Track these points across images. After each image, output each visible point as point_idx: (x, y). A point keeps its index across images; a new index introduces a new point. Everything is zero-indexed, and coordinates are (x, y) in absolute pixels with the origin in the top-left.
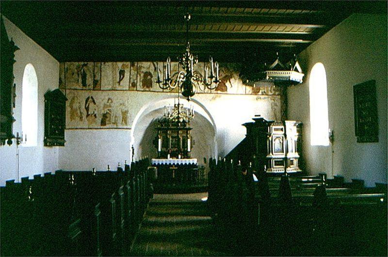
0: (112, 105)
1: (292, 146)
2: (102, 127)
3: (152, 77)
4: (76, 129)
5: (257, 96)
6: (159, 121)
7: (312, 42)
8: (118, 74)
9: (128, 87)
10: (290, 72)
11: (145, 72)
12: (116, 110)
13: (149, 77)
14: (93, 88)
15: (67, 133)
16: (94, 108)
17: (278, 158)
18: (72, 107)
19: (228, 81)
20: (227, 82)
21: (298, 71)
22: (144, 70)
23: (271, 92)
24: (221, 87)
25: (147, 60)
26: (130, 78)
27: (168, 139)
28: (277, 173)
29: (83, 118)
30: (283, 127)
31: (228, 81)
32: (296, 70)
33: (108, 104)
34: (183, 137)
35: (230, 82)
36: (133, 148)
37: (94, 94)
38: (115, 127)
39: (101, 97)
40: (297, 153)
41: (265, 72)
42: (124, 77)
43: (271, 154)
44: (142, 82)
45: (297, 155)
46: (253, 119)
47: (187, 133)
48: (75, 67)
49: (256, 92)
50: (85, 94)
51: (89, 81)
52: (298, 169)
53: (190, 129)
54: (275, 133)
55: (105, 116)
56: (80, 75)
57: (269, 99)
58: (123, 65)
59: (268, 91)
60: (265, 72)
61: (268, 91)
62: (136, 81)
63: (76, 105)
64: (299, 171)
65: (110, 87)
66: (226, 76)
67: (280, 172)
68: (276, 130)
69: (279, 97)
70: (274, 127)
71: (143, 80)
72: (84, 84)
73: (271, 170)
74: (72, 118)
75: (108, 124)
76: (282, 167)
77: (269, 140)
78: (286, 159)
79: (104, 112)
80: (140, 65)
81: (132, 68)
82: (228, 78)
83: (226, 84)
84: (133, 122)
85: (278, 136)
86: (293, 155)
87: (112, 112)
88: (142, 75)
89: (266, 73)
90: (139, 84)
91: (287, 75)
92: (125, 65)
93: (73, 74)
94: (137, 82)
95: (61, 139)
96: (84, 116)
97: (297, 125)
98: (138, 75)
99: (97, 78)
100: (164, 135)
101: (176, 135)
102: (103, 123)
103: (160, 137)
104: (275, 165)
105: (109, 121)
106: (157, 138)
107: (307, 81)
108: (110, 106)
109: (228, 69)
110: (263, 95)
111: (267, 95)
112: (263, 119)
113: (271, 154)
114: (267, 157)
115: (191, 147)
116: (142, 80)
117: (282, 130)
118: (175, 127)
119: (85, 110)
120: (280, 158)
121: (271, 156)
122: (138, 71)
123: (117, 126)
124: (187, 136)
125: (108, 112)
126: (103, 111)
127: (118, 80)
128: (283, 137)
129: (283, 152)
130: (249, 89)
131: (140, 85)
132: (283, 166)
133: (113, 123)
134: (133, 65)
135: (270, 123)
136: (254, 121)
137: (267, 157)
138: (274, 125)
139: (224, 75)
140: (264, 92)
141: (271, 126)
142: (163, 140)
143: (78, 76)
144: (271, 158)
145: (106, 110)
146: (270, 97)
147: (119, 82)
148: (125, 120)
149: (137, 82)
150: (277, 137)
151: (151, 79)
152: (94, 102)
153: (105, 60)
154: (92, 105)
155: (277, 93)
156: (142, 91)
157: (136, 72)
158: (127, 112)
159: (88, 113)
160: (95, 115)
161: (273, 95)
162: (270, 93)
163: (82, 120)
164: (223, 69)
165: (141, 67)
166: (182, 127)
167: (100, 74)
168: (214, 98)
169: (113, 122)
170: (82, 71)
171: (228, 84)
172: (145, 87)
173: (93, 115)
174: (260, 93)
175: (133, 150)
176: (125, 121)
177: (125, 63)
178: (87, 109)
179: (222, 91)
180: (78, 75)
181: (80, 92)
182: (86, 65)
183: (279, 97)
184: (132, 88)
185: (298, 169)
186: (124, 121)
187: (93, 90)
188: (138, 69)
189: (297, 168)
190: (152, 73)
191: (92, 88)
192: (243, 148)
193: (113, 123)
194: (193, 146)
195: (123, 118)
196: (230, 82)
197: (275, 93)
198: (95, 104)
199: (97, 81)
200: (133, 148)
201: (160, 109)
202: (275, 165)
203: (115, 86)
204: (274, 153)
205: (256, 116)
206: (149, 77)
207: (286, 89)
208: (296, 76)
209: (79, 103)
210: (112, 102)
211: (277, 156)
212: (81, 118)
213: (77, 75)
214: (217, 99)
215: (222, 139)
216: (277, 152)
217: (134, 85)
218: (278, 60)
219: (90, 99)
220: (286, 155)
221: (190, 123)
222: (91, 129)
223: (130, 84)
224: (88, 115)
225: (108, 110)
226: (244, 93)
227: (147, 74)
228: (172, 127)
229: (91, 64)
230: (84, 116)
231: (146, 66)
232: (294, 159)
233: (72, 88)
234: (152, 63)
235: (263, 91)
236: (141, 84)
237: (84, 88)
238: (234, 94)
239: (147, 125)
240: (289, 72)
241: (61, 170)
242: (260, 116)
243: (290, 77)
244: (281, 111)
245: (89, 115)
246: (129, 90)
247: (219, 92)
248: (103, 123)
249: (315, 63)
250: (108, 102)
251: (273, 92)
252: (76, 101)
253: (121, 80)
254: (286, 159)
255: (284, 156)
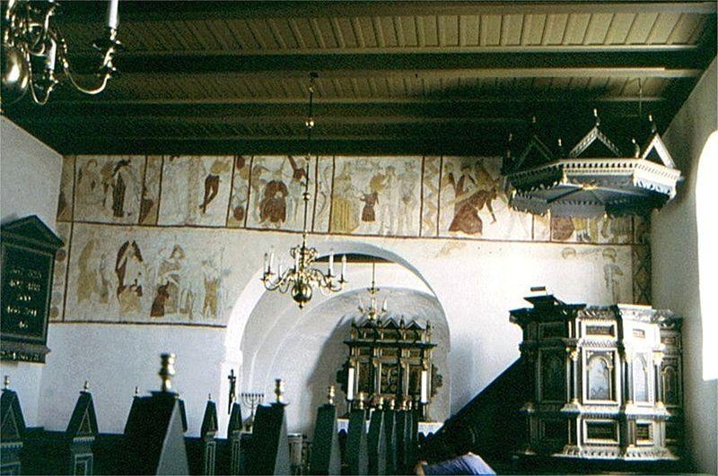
0: (183, 262)
1: (644, 379)
2: (153, 319)
3: (286, 194)
4: (90, 322)
5: (565, 246)
6: (354, 325)
7: (695, 71)
8: (202, 185)
9: (225, 220)
10: (633, 161)
11: (269, 181)
12: (191, 279)
13: (279, 194)
14: (141, 219)
15: (55, 333)
16: (139, 270)
17: (598, 416)
18: (83, 266)
19: (485, 205)
20: (481, 208)
21: (660, 162)
22: (267, 176)
23: (605, 236)
24: (466, 220)
25: (273, 150)
26: (231, 198)
27: (374, 370)
28: (594, 460)
29: (110, 296)
30: (614, 323)
31: (485, 205)
32: (654, 157)
33: (173, 261)
34: (411, 366)
35: (490, 209)
36: (232, 378)
37: (140, 235)
38: (187, 321)
39: (156, 244)
40: (660, 404)
41: (557, 165)
42: (215, 192)
43: (576, 402)
44: (261, 208)
45: (661, 410)
46: (527, 299)
47: (422, 355)
48: (100, 167)
49: (561, 235)
50: (122, 236)
51: (132, 203)
52: (664, 453)
53: (429, 346)
54: (589, 340)
55: (163, 291)
56: (110, 188)
57: (600, 253)
58: (216, 163)
59: (594, 234)
60: (557, 165)
61: (594, 234)
62: (245, 205)
63: (94, 263)
64: (669, 457)
65: (180, 219)
66: (481, 193)
67: (603, 457)
68: (590, 330)
69: (628, 249)
70: (585, 323)
71: (263, 201)
72: (118, 209)
73: (577, 451)
74: (83, 293)
75: (168, 312)
76: (612, 442)
77: (572, 362)
78: (621, 418)
79: (162, 280)
80: (258, 163)
81: (237, 171)
82: (483, 198)
83: (480, 214)
84: (231, 307)
85: (596, 349)
86: (646, 407)
87: (181, 282)
88: (262, 188)
89: (561, 166)
90: (253, 212)
91: (624, 172)
92: (221, 163)
93: (93, 185)
94: (248, 205)
95: (37, 343)
96: (112, 292)
97: (662, 319)
98: (252, 190)
99: (152, 194)
100: (365, 359)
101: (395, 362)
102: (157, 309)
103: (353, 364)
104: (589, 437)
105: (174, 305)
106: (347, 366)
107: (691, 192)
108: (177, 268)
109: (484, 171)
110: (581, 242)
111: (593, 244)
112: (551, 298)
113: (576, 402)
114: (565, 409)
115: (432, 393)
116: (260, 200)
117: (610, 331)
118: (393, 341)
119: (115, 275)
120: (606, 416)
121: (575, 406)
122: (252, 177)
123: (191, 318)
124: (422, 364)
125: (172, 280)
126: (159, 279)
127: (201, 200)
128: (613, 352)
129: (614, 399)
130: (542, 226)
131: (254, 212)
132: (616, 440)
133: (181, 310)
134: (240, 164)
135: (573, 310)
136: (530, 306)
137: (565, 409)
138: (587, 317)
139: (473, 191)
140: (586, 236)
141: (577, 320)
142: (362, 373)
143: (106, 191)
144: (574, 416)
145: (165, 278)
146: (603, 248)
147: (204, 207)
148: (211, 302)
149: (248, 205)
150: (596, 354)
151: (283, 199)
152: (138, 254)
153: (176, 149)
154: (132, 263)
155: (621, 239)
156: (260, 230)
157: (247, 182)
158: (216, 283)
159: (121, 283)
160: (139, 290)
161: (608, 244)
162: (601, 239)
163: (106, 302)
164: (473, 175)
165: (259, 170)
166: (411, 342)
167: (157, 185)
168: (445, 252)
169: (184, 307)
170: (116, 177)
171: (483, 214)
172: (267, 220)
173: (135, 288)
174: (574, 238)
175: (233, 385)
176: (211, 305)
177: (220, 158)
178: (121, 272)
179: (468, 233)
180: (106, 187)
181: (107, 230)
182: (124, 163)
183: (628, 249)
184: (236, 223)
185: (664, 453)
186: (208, 307)
187: (139, 225)
188: (252, 175)
189: (663, 449)
190: (287, 184)
191: (137, 222)
192: (514, 382)
193: (181, 310)
194: (438, 389)
195: (207, 298)
196: (490, 209)
197: (616, 238)
198: (141, 260)
199: (151, 203)
200: (232, 378)
201: (356, 293)
202: (589, 437)
203: (192, 217)
204: (585, 401)
205: (532, 290)
206: (279, 194)
207: (647, 223)
208: (653, 174)
209: (103, 257)
210: (182, 257)
211: (589, 407)
212: (104, 295)
213: (102, 187)
214: (454, 252)
215: (465, 362)
216: (592, 399)
217: (240, 214)
218: (595, 129)
219: (130, 249)
220: (623, 407)
221: (432, 330)
222: (125, 323)
223: (231, 213)
224: (121, 289)
225: (172, 276)
226: (530, 239)
227: (275, 186)
228: (387, 341)
229: (138, 161)
230: (112, 292)
231: (274, 166)
232: (654, 423)
233: (87, 219)
234: (288, 160)
235: (582, 232)
236: (258, 211)
237: (118, 220)
238: (500, 241)
239: (327, 334)
240: (628, 162)
241: (42, 428)
242: (543, 289)
243: (632, 176)
244: (634, 290)
245: (125, 287)
246: (226, 227)
247: (460, 234)
248: (157, 309)
249: (709, 134)
250: (172, 256)
251: (612, 236)
252: (94, 251)
253: (207, 201)
254: (621, 418)
255: (615, 411)
